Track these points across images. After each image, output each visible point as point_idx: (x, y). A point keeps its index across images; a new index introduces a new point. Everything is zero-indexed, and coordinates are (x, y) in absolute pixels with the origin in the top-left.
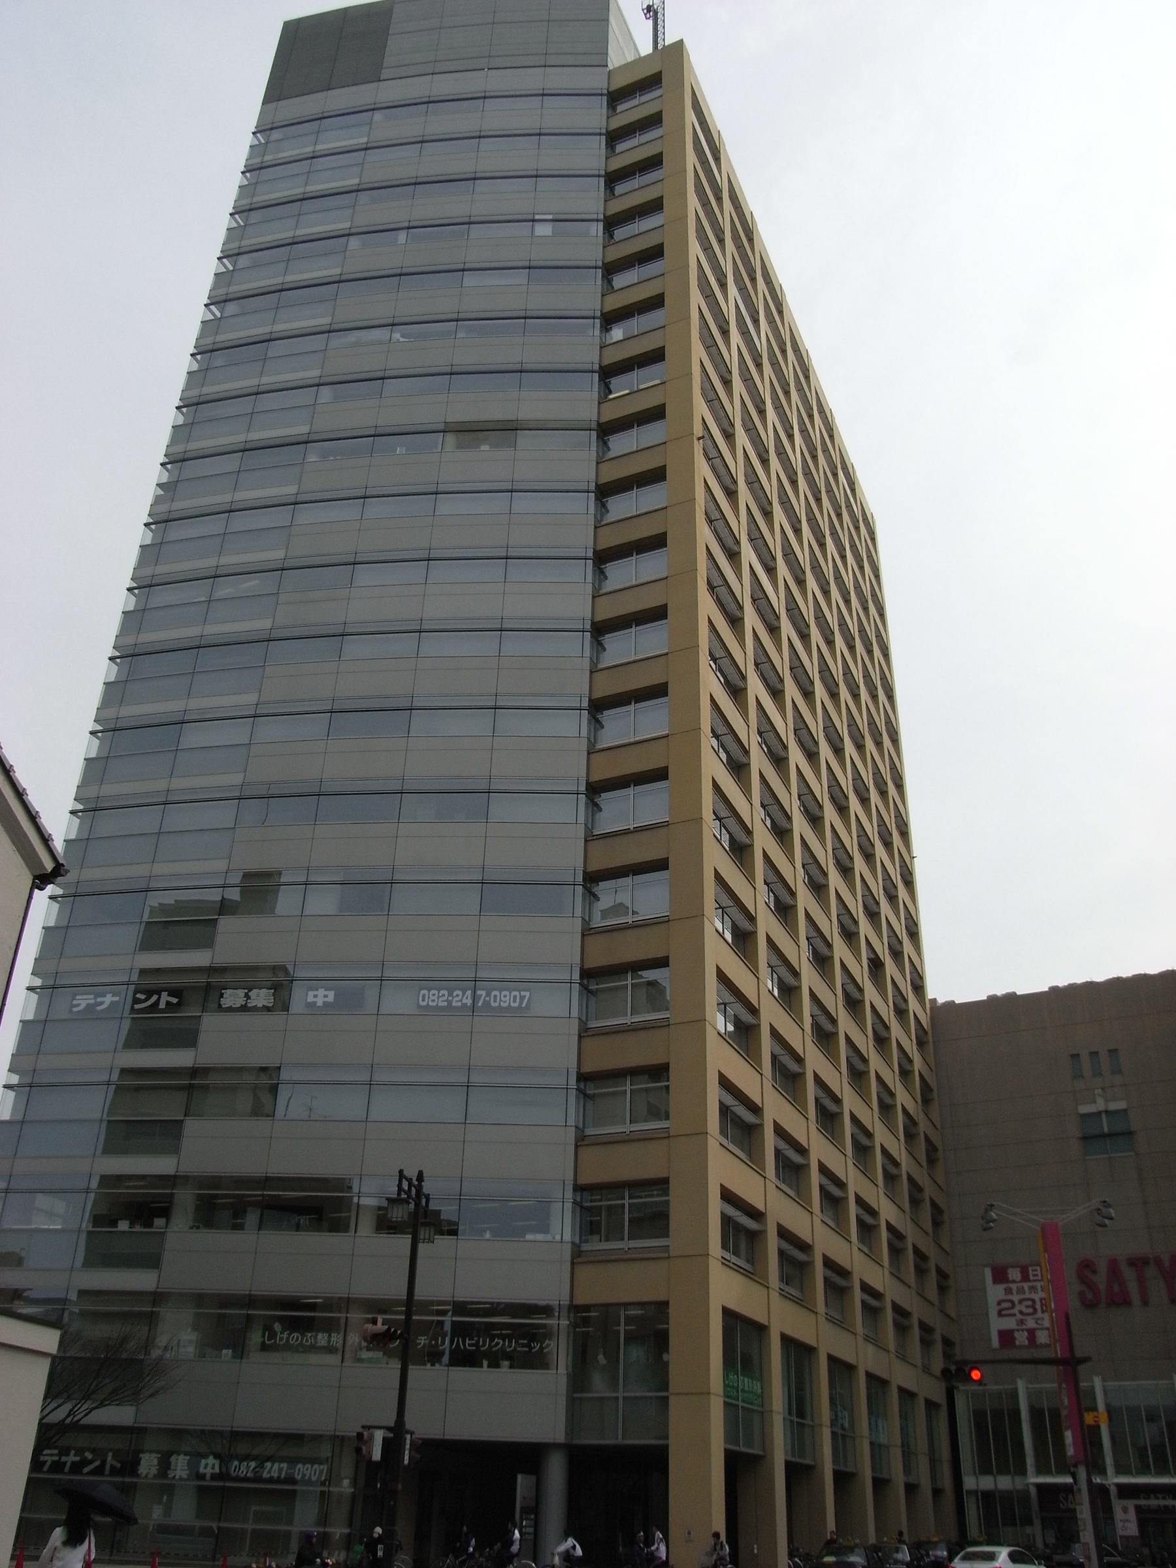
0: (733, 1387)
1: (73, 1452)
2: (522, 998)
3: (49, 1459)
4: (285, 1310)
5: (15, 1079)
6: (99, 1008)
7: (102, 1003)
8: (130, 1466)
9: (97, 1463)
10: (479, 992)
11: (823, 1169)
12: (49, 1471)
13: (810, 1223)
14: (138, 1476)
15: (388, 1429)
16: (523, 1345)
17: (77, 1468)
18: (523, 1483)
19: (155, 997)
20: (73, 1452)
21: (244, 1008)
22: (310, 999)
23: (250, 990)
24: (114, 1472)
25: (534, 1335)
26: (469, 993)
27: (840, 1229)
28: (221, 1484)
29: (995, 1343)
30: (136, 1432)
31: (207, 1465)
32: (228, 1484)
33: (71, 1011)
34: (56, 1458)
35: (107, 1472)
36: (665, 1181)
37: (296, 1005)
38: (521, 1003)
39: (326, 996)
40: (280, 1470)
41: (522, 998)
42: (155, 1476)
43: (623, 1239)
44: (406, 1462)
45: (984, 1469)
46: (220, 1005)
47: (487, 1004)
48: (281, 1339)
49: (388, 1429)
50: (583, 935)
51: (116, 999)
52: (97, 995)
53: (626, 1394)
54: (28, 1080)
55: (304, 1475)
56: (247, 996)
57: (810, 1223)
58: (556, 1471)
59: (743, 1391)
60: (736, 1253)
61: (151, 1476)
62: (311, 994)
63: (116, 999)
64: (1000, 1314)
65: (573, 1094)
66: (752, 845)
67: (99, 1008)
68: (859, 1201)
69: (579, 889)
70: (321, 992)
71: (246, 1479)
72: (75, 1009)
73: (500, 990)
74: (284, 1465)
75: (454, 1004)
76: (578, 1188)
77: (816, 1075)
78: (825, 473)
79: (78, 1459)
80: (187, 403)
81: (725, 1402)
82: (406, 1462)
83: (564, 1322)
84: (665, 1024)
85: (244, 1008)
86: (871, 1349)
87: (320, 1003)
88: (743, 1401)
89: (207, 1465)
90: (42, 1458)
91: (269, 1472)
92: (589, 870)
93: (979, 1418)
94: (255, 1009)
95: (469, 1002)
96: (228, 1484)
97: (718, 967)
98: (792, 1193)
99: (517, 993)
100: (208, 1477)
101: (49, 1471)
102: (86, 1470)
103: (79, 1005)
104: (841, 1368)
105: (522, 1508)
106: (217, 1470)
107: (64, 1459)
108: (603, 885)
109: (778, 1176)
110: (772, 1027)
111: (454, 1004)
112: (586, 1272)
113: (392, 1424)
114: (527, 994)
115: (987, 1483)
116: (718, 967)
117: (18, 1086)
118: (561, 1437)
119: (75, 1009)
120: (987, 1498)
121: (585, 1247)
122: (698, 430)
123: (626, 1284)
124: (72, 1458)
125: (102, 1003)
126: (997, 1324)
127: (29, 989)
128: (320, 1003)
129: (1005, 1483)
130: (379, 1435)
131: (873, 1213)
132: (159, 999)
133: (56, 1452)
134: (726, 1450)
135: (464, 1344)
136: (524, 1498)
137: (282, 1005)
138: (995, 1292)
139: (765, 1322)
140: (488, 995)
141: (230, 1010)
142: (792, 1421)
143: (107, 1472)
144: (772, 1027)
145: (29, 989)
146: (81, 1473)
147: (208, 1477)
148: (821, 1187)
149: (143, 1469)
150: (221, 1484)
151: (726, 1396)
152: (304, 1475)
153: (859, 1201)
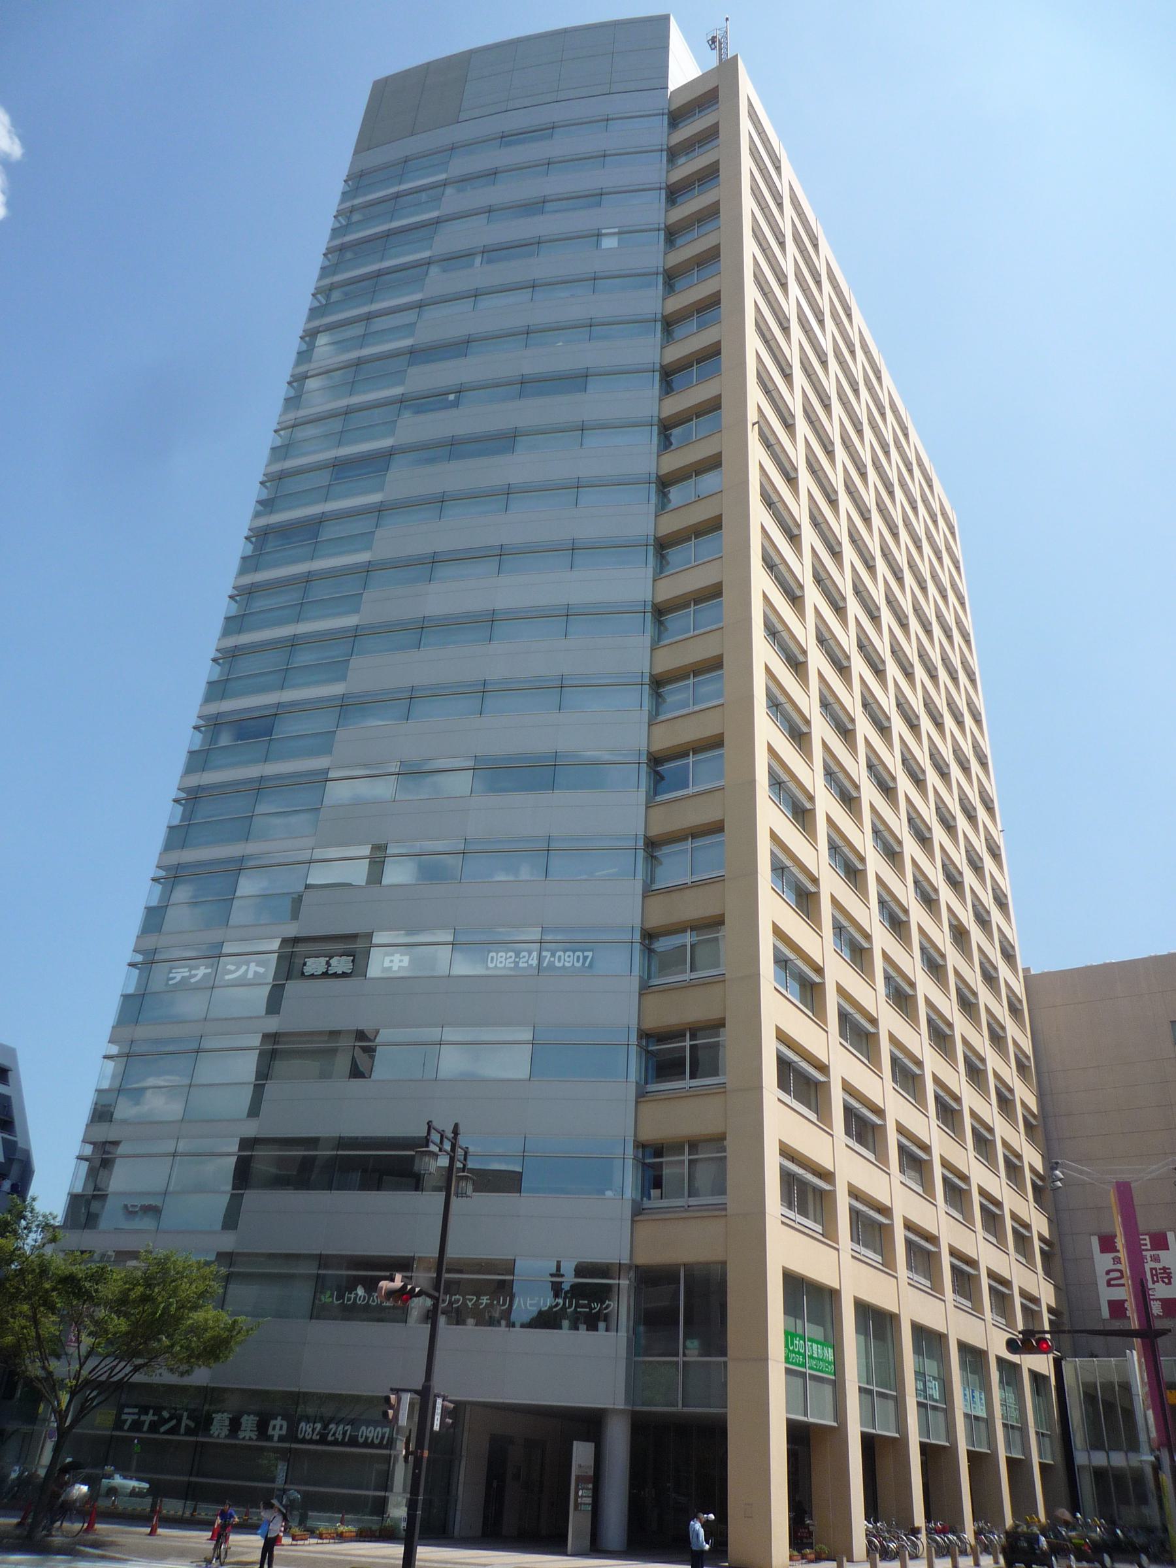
0: (799, 1353)
1: (151, 1412)
2: (585, 958)
3: (130, 1418)
4: (357, 1270)
5: (114, 1050)
6: (193, 980)
7: (195, 975)
8: (203, 1423)
9: (174, 1422)
10: (544, 953)
11: (983, 1192)
12: (129, 1430)
13: (937, 1218)
14: (211, 1436)
15: (416, 1392)
16: (583, 1306)
17: (154, 1427)
18: (582, 1454)
19: (244, 968)
20: (151, 1412)
21: (325, 975)
22: (387, 964)
23: (331, 957)
24: (189, 1431)
25: (602, 1294)
26: (535, 954)
27: (1001, 1244)
28: (287, 1445)
29: (1105, 1313)
30: (210, 1394)
31: (281, 1429)
32: (294, 1446)
33: (167, 984)
34: (136, 1417)
35: (182, 1430)
36: (722, 1138)
37: (374, 971)
38: (584, 963)
39: (401, 961)
40: (344, 1434)
41: (585, 958)
42: (226, 1437)
43: (682, 1196)
44: (436, 1427)
45: (1096, 1444)
46: (303, 974)
47: (551, 966)
48: (349, 1299)
49: (416, 1392)
50: (644, 897)
51: (209, 970)
52: (191, 968)
53: (675, 1359)
54: (126, 1050)
55: (367, 1438)
56: (328, 963)
57: (937, 1218)
58: (618, 1437)
59: (811, 1357)
60: (803, 1212)
61: (223, 1435)
62: (387, 959)
63: (209, 970)
64: (1109, 1285)
65: (637, 946)
66: (865, 870)
67: (193, 980)
68: (1014, 1217)
69: (641, 853)
70: (397, 957)
71: (311, 1442)
72: (171, 982)
73: (565, 951)
74: (348, 1427)
75: (521, 965)
76: (640, 1146)
77: (971, 1111)
78: (903, 507)
79: (156, 1418)
80: (284, 425)
81: (786, 1369)
82: (436, 1427)
83: (624, 1282)
84: (720, 879)
85: (325, 975)
86: (246, 1067)
87: (395, 968)
88: (810, 1368)
89: (281, 1429)
90: (124, 1417)
91: (334, 1434)
92: (650, 834)
93: (1090, 1397)
94: (335, 975)
95: (535, 962)
96: (294, 1446)
97: (774, 924)
98: (921, 1192)
99: (580, 953)
100: (276, 1438)
101: (129, 1430)
102: (162, 1429)
103: (173, 978)
104: (929, 1340)
105: (578, 1477)
106: (284, 1432)
107: (143, 1418)
108: (666, 850)
109: (946, 1201)
110: (934, 1075)
111: (521, 965)
112: (646, 1230)
113: (420, 1388)
114: (590, 954)
115: (1100, 1459)
116: (774, 924)
117: (117, 1056)
118: (620, 1405)
119: (171, 982)
120: (1100, 1475)
121: (647, 1204)
122: (752, 416)
123: (682, 1243)
124: (149, 1418)
125: (195, 975)
126: (1107, 1295)
127: (130, 965)
128: (395, 968)
129: (1118, 1460)
130: (406, 1398)
131: (1027, 1227)
132: (247, 970)
133: (136, 1410)
134: (788, 1420)
135: (525, 1304)
136: (580, 1466)
137: (359, 968)
138: (1103, 1262)
139: (835, 1285)
140: (553, 955)
141: (312, 976)
142: (870, 1392)
143: (182, 1430)
144: (934, 1075)
145: (130, 965)
146: (158, 1432)
147: (276, 1438)
148: (1013, 1228)
149: (215, 1429)
150: (287, 1445)
151: (787, 1360)
152: (367, 1438)
153: (1014, 1217)
